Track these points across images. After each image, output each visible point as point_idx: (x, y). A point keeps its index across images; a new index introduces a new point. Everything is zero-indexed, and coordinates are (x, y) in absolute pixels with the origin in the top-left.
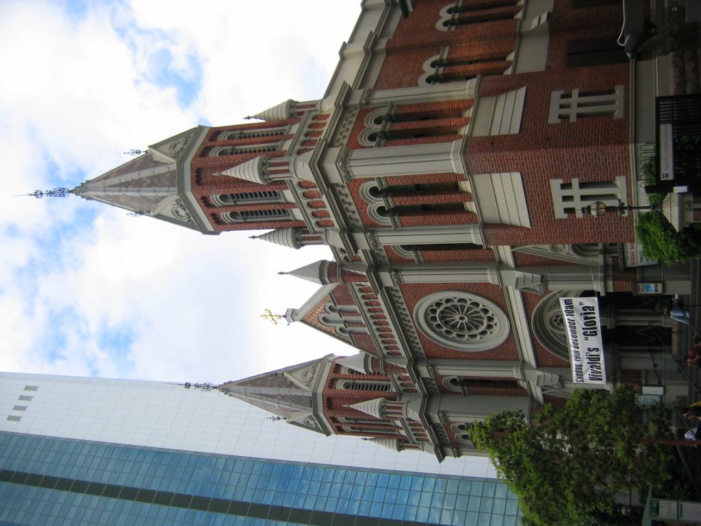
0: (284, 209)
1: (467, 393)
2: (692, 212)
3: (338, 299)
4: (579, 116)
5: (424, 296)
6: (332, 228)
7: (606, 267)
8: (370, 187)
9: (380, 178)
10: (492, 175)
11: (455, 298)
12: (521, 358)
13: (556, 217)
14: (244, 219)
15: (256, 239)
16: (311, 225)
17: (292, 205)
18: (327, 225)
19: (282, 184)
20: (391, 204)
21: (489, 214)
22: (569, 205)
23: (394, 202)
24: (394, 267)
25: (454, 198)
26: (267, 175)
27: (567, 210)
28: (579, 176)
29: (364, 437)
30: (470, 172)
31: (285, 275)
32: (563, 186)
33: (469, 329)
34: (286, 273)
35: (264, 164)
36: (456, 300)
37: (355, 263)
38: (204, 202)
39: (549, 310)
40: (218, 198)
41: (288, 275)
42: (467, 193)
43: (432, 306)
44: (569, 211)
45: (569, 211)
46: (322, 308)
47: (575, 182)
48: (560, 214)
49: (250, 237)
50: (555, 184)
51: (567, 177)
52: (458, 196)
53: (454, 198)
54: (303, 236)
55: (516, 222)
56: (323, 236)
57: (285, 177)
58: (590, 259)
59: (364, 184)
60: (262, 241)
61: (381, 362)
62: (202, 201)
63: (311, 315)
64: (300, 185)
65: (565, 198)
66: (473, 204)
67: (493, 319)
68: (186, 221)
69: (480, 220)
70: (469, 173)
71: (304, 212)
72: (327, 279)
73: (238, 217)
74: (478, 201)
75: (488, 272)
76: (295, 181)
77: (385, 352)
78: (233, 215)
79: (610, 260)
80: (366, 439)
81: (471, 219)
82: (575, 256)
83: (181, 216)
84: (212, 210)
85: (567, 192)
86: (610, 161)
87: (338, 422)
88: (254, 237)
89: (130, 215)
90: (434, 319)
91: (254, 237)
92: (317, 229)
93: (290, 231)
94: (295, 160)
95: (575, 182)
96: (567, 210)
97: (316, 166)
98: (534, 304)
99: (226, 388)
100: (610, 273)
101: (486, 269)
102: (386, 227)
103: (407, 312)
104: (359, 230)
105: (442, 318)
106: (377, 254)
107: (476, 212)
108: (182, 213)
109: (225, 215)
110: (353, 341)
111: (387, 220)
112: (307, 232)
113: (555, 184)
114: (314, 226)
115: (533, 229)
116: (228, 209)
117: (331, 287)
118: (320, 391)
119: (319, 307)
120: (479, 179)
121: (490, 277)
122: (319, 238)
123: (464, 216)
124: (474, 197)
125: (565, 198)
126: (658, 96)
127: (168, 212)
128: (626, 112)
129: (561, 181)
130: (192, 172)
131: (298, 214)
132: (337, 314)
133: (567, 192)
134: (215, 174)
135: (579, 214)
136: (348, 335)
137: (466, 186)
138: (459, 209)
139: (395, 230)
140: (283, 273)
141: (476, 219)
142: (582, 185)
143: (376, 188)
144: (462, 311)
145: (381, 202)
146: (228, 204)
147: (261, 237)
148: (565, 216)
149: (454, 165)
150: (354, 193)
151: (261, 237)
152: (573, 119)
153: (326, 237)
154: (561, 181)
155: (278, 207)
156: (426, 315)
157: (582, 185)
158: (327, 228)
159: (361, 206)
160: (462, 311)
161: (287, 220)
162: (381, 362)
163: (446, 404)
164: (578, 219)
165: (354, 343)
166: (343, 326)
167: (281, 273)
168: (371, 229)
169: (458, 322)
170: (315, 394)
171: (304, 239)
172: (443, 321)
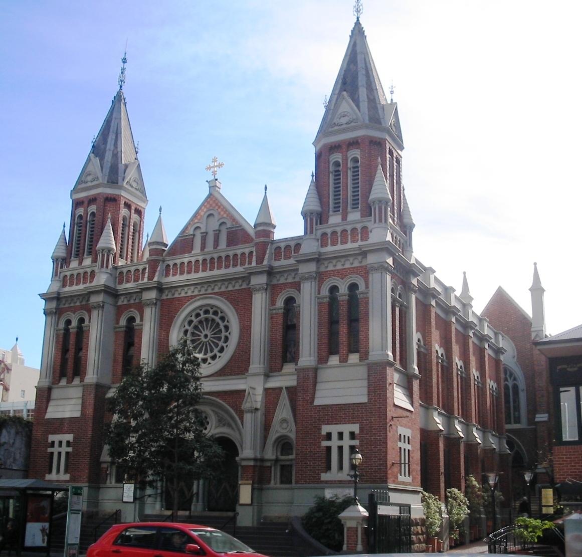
0: (79, 255)
1: (118, 330)
2: (355, 526)
3: (236, 233)
4: (329, 449)
5: (234, 308)
6: (320, 245)
7: (262, 460)
8: (358, 284)
9: (368, 293)
10: (367, 381)
11: (230, 334)
12: (271, 374)
13: (322, 426)
14: (77, 222)
15: (63, 227)
16: (325, 228)
17: (80, 263)
18: (323, 243)
19: (95, 260)
20: (341, 297)
21: (324, 374)
22: (335, 436)
23: (343, 301)
24: (158, 303)
25: (70, 371)
26: (379, 204)
27: (53, 443)
28: (361, 446)
29: (314, 175)
30: (85, 387)
31: (264, 191)
32: (68, 442)
33: (219, 339)
34: (266, 193)
35: (380, 201)
36: (227, 334)
37: (273, 255)
38: (80, 203)
39: (213, 411)
40: (80, 213)
41: (264, 194)
42: (72, 381)
43: (221, 313)
44: (329, 436)
45: (329, 436)
46: (225, 216)
47: (70, 449)
48: (325, 429)
49: (64, 224)
50: (356, 428)
51: (361, 437)
52: (71, 375)
53: (343, 349)
54: (314, 219)
55: (318, 394)
56: (57, 278)
57: (375, 215)
58: (271, 448)
59: (362, 279)
60: (60, 233)
61: (160, 258)
62: (94, 198)
63: (217, 205)
64: (93, 273)
65: (60, 442)
66: (65, 384)
67: (205, 363)
68: (83, 179)
69: (54, 386)
70: (84, 386)
71: (74, 269)
72: (154, 247)
73: (78, 219)
74: (338, 367)
75: (262, 366)
76: (96, 269)
77: (171, 263)
78: (80, 217)
79: (268, 464)
80: (313, 176)
81: (322, 360)
82: (273, 439)
83: (340, 119)
84: (86, 203)
85: (64, 444)
86: (374, 470)
87: (89, 205)
88: (64, 226)
89: (93, 137)
90: (207, 312)
91: (64, 226)
92: (319, 233)
93: (319, 209)
94: (382, 227)
95: (70, 449)
96: (53, 443)
97: (387, 246)
98: (224, 400)
99: (358, 33)
100: (258, 464)
101: (97, 375)
102: (58, 324)
103: (216, 290)
104: (58, 305)
105: (207, 320)
106: (283, 276)
107: (72, 384)
108: (344, 120)
109: (81, 211)
110: (184, 236)
111: (325, 292)
112: (62, 267)
113: (356, 428)
114: (323, 230)
115: (313, 407)
116: (85, 215)
117: (251, 232)
118: (123, 193)
119: (225, 213)
120: (80, 390)
121: (257, 364)
122: (56, 275)
123: (324, 354)
124: (342, 364)
125: (60, 442)
126: (411, 506)
127: (90, 168)
128: (404, 483)
129: (357, 431)
130: (379, 138)
131: (74, 264)
132: (217, 228)
133: (64, 444)
134: (110, 215)
135: (356, 443)
136: (192, 233)
137: (77, 381)
138: (63, 374)
139: (316, 297)
140: (160, 211)
141: (322, 363)
142: (67, 453)
143: (84, 323)
144: (214, 338)
145: (74, 323)
146: (76, 219)
147: (64, 232)
148: (324, 432)
149: (91, 377)
150: (354, 271)
151: (64, 232)
152: (50, 450)
153: (312, 238)
154: (357, 431)
155: (81, 251)
156: (212, 306)
157: (67, 453)
158: (320, 241)
159: (342, 274)
160: (214, 338)
161: (84, 253)
162: (160, 258)
163: (109, 309)
164: (321, 442)
165: (182, 237)
166: (203, 230)
167: (160, 209)
168: (320, 277)
169: (202, 333)
170: (121, 188)
171: (311, 220)
172: (203, 319)
